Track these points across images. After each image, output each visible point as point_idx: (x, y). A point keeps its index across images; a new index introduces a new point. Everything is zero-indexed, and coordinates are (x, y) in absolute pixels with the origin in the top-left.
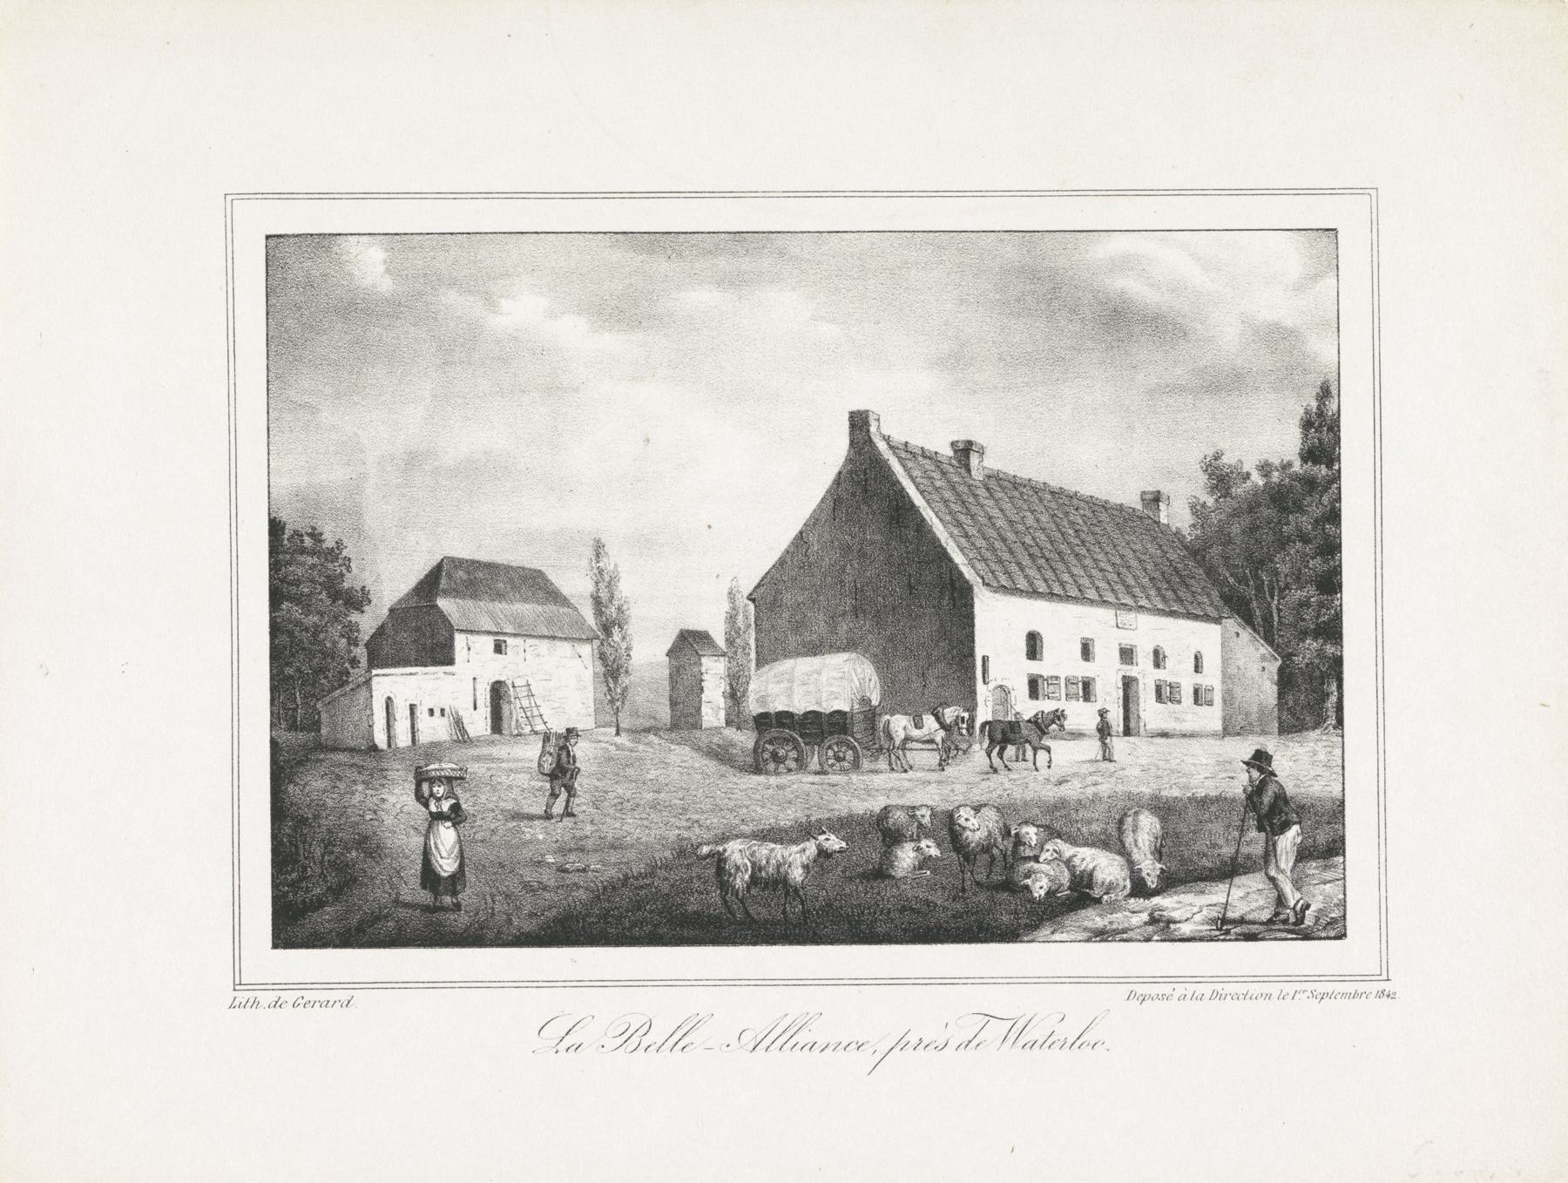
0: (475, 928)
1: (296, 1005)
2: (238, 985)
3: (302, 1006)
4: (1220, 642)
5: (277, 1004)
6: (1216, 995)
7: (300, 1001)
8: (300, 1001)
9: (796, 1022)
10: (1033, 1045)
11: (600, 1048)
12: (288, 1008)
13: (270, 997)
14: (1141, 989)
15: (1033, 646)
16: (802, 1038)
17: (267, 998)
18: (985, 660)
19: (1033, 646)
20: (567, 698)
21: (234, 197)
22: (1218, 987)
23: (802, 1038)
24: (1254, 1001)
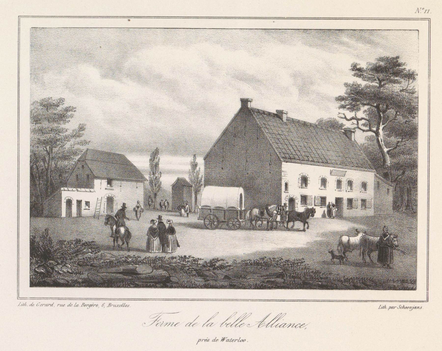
0: (35, 278)
1: (38, 305)
2: (18, 297)
3: (39, 305)
4: (29, 160)
5: (70, 305)
6: (84, 305)
7: (38, 304)
8: (39, 304)
9: (242, 317)
10: (172, 325)
11: (248, 326)
12: (73, 307)
13: (30, 302)
14: (87, 302)
15: (305, 180)
16: (280, 322)
17: (29, 302)
18: (286, 185)
19: (305, 180)
20: (348, 209)
21: (20, 17)
22: (110, 302)
23: (280, 322)
24: (125, 307)
